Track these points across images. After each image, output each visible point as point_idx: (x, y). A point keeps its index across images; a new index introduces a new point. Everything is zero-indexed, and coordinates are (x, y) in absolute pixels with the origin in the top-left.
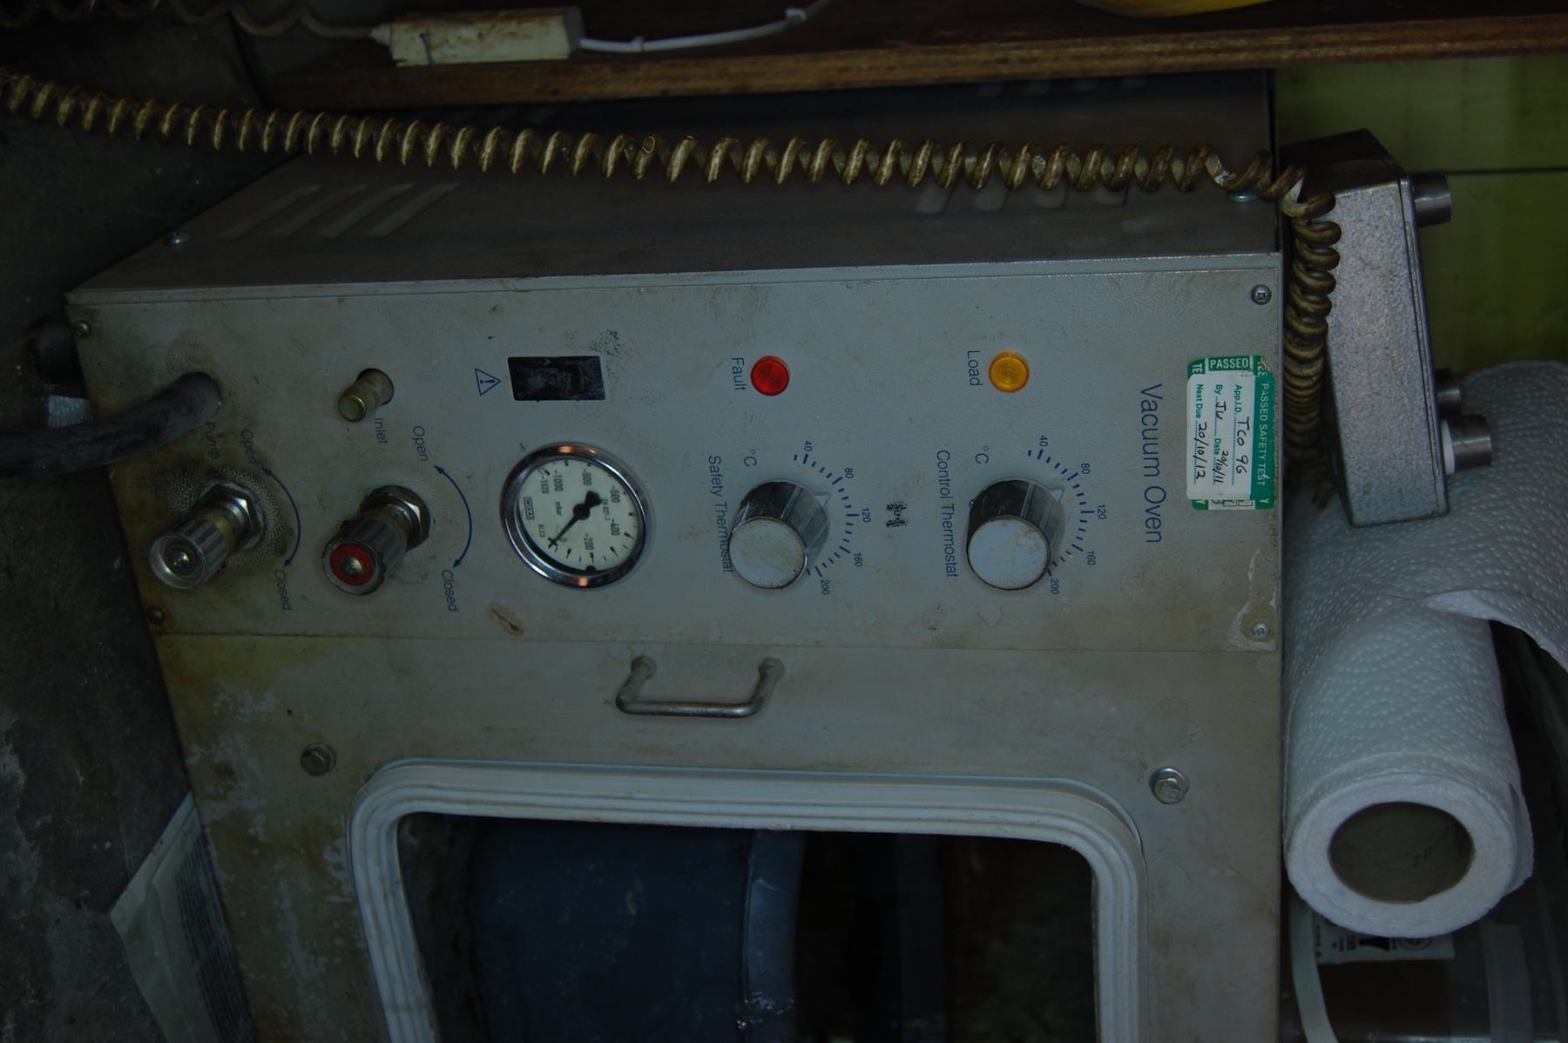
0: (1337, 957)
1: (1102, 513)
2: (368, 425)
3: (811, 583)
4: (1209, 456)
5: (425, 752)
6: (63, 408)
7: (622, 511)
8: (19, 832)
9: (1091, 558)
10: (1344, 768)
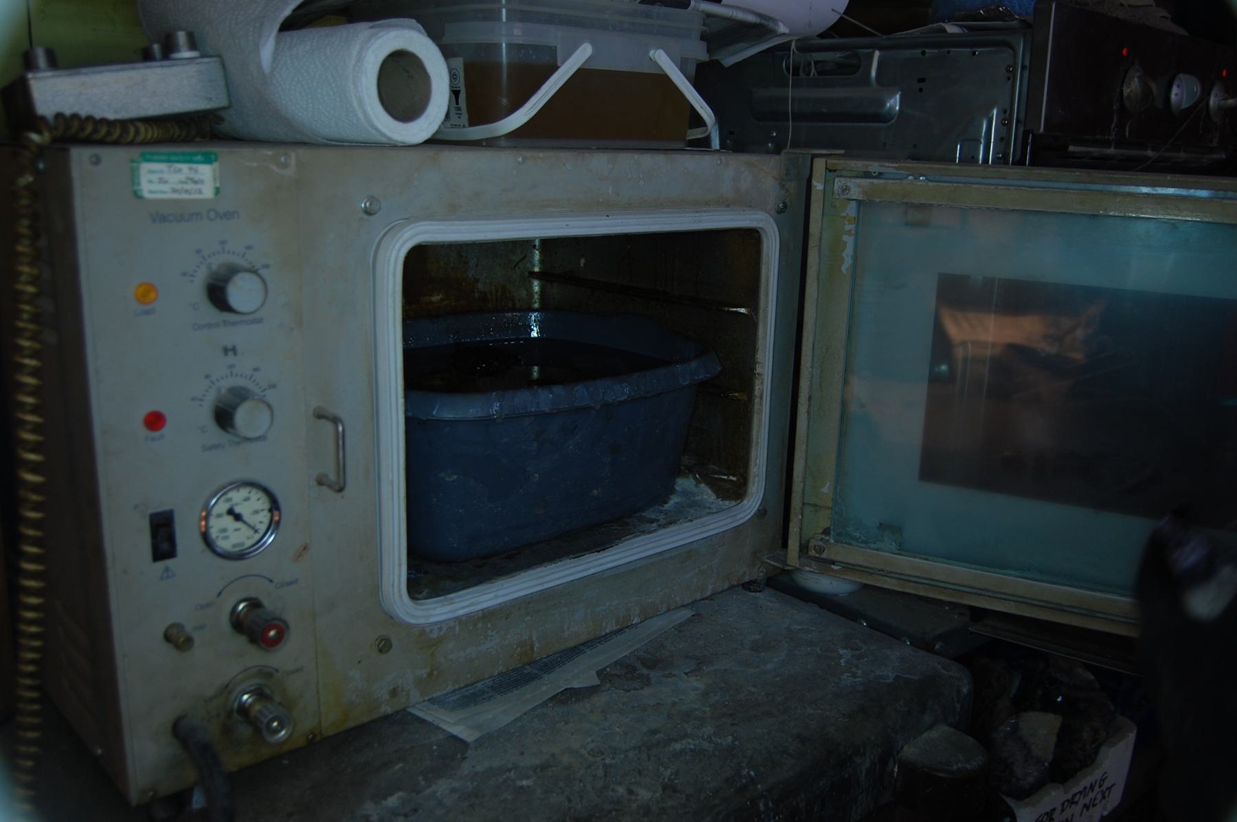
0: (465, 116)
1: (223, 243)
2: (196, 636)
3: (271, 396)
4: (190, 186)
5: (376, 589)
6: (198, 801)
7: (237, 496)
8: (428, 791)
9: (249, 248)
10: (361, 115)
